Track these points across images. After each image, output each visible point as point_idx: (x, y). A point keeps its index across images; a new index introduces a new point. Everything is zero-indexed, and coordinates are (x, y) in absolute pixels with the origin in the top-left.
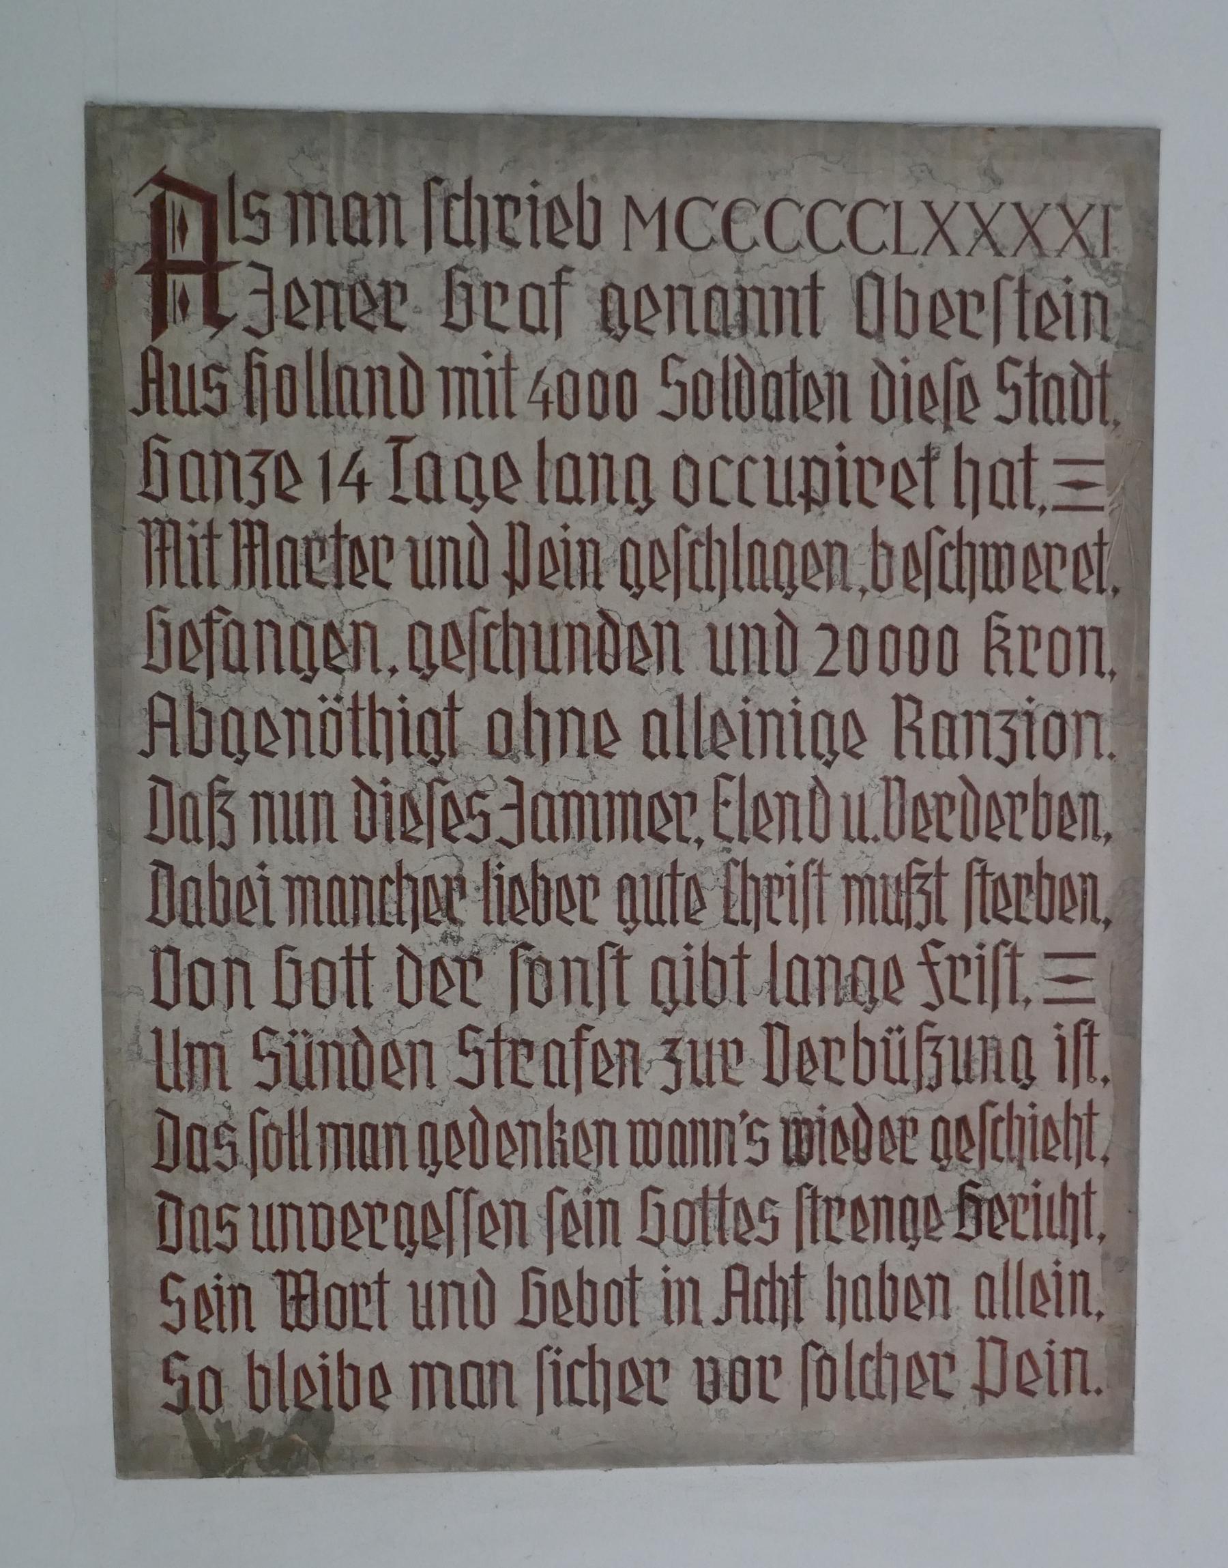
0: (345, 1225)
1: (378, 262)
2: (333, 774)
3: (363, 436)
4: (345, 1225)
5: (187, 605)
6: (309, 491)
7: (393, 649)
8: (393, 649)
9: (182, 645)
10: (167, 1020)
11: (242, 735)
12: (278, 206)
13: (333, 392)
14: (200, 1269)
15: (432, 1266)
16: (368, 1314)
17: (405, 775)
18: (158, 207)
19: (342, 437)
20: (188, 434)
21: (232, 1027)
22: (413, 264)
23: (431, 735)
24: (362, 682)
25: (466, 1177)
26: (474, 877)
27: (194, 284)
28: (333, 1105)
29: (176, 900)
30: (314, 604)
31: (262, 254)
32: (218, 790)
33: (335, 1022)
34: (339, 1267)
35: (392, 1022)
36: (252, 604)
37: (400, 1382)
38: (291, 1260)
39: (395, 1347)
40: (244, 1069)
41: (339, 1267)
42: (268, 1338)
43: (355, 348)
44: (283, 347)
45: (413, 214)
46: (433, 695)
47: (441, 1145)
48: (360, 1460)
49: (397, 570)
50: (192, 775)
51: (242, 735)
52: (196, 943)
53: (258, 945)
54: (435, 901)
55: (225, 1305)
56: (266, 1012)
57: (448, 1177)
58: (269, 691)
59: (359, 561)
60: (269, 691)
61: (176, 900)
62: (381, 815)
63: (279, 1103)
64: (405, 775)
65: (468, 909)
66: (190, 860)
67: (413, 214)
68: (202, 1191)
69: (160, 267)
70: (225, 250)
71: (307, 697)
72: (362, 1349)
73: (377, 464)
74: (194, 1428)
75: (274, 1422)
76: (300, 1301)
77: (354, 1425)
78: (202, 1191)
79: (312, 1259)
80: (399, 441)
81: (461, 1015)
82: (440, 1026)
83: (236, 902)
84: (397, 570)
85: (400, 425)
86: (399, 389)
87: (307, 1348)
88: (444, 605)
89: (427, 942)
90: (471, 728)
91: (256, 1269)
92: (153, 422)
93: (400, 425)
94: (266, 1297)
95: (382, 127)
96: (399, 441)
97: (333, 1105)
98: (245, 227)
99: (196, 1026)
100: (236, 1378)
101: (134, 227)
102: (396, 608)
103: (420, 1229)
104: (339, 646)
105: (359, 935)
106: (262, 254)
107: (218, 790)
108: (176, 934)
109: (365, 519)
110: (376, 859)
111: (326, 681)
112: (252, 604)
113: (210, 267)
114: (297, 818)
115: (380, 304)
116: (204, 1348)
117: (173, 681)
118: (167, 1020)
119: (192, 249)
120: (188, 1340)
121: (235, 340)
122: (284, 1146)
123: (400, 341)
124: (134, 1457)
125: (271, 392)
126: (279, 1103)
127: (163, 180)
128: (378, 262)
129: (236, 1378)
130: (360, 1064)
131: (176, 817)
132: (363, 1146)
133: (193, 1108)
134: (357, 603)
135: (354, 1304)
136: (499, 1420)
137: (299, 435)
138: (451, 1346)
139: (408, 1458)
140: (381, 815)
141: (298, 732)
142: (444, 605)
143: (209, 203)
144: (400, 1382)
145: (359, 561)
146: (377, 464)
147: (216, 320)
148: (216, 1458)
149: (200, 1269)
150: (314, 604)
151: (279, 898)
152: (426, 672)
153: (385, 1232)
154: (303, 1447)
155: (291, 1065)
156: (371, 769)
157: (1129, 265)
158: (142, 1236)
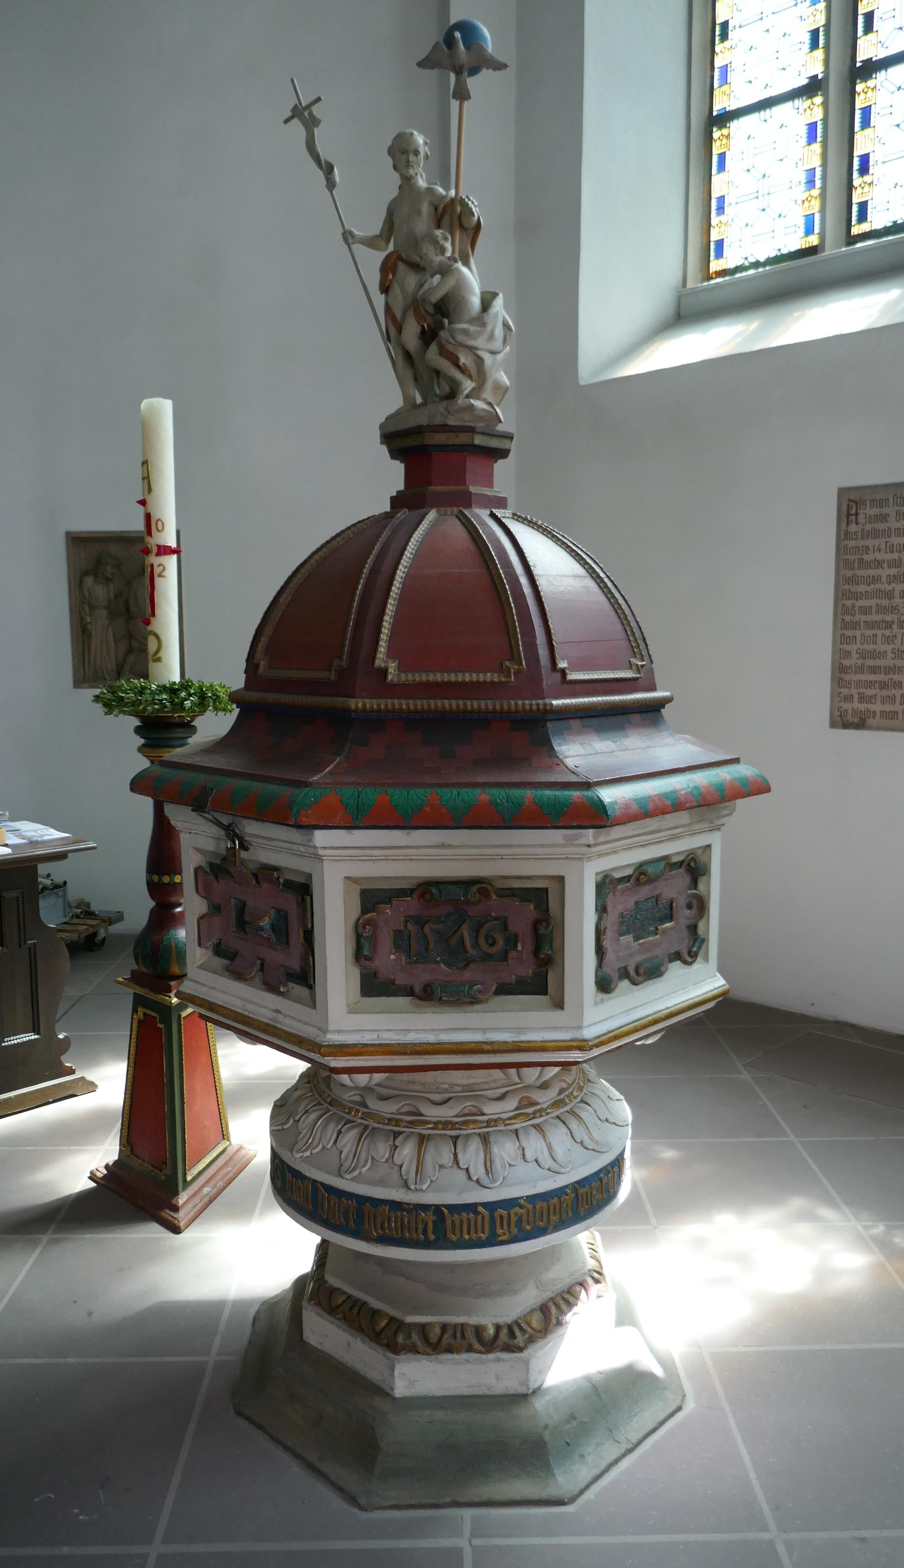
0: (870, 684)
1: (885, 510)
2: (872, 603)
3: (880, 542)
4: (870, 684)
5: (850, 573)
6: (871, 552)
7: (884, 579)
8: (884, 579)
9: (849, 580)
10: (842, 647)
11: (857, 596)
12: (868, 503)
13: (875, 534)
14: (845, 691)
15: (885, 693)
16: (873, 701)
17: (885, 602)
18: (848, 505)
19: (877, 542)
20: (851, 544)
21: (853, 648)
22: (890, 510)
23: (890, 595)
24: (878, 586)
25: (891, 676)
26: (896, 621)
27: (853, 518)
28: (870, 662)
29: (845, 625)
30: (870, 572)
31: (866, 511)
32: (853, 606)
33: (871, 647)
34: (869, 692)
35: (881, 647)
36: (860, 573)
37: (878, 714)
38: (861, 691)
39: (877, 707)
40: (855, 656)
41: (869, 692)
42: (856, 705)
43: (881, 526)
44: (868, 527)
45: (891, 501)
46: (890, 588)
47: (888, 670)
48: (870, 728)
49: (885, 565)
50: (849, 603)
51: (857, 596)
52: (849, 633)
53: (858, 633)
54: (889, 625)
55: (849, 698)
56: (859, 645)
57: (888, 676)
58: (862, 588)
59: (879, 564)
60: (862, 588)
61: (845, 625)
62: (881, 610)
63: (860, 662)
64: (885, 602)
65: (895, 627)
66: (848, 618)
67: (891, 501)
68: (847, 677)
69: (848, 515)
70: (859, 511)
71: (869, 589)
72: (872, 707)
73: (883, 547)
74: (843, 720)
75: (856, 720)
76: (862, 698)
77: (870, 721)
78: (847, 677)
79: (864, 690)
80: (887, 542)
81: (892, 646)
82: (888, 648)
83: (855, 626)
84: (885, 565)
85: (887, 539)
86: (888, 533)
87: (863, 707)
88: (894, 571)
89: (887, 633)
90: (897, 594)
91: (854, 692)
92: (846, 542)
93: (887, 539)
94: (856, 697)
95: (887, 486)
96: (887, 542)
97: (870, 662)
98: (863, 507)
99: (847, 648)
100: (850, 711)
101: (845, 509)
102: (885, 572)
103: (884, 686)
104: (875, 579)
105: (875, 632)
106: (866, 511)
107: (853, 606)
108: (845, 632)
109: (880, 556)
110: (879, 618)
111: (872, 586)
112: (860, 573)
113: (856, 514)
114: (865, 611)
115: (884, 518)
116: (846, 706)
117: (847, 587)
118: (842, 647)
119: (853, 511)
120: (842, 704)
121: (860, 527)
122: (860, 670)
123: (887, 524)
124: (833, 725)
125: (865, 535)
126: (860, 662)
127: (850, 500)
128: (885, 510)
129: (850, 711)
130: (875, 655)
131: (846, 610)
132: (874, 670)
133: (846, 662)
134: (878, 572)
135: (871, 699)
136: (895, 723)
137: (869, 542)
138: (887, 708)
139: (879, 728)
140: (881, 610)
141: (867, 595)
142: (894, 571)
143: (857, 503)
144: (878, 714)
145: (879, 564)
146: (883, 547)
147: (857, 523)
148: (846, 726)
149: (845, 691)
150: (870, 572)
151: (862, 624)
152: (889, 583)
153: (877, 686)
154: (861, 725)
155: (862, 655)
156: (879, 601)
157: (243, 862)
158: (837, 685)
